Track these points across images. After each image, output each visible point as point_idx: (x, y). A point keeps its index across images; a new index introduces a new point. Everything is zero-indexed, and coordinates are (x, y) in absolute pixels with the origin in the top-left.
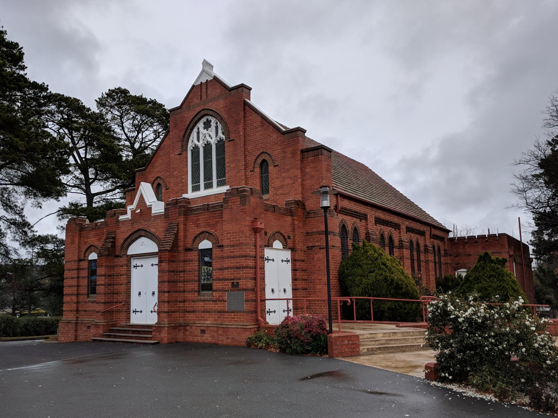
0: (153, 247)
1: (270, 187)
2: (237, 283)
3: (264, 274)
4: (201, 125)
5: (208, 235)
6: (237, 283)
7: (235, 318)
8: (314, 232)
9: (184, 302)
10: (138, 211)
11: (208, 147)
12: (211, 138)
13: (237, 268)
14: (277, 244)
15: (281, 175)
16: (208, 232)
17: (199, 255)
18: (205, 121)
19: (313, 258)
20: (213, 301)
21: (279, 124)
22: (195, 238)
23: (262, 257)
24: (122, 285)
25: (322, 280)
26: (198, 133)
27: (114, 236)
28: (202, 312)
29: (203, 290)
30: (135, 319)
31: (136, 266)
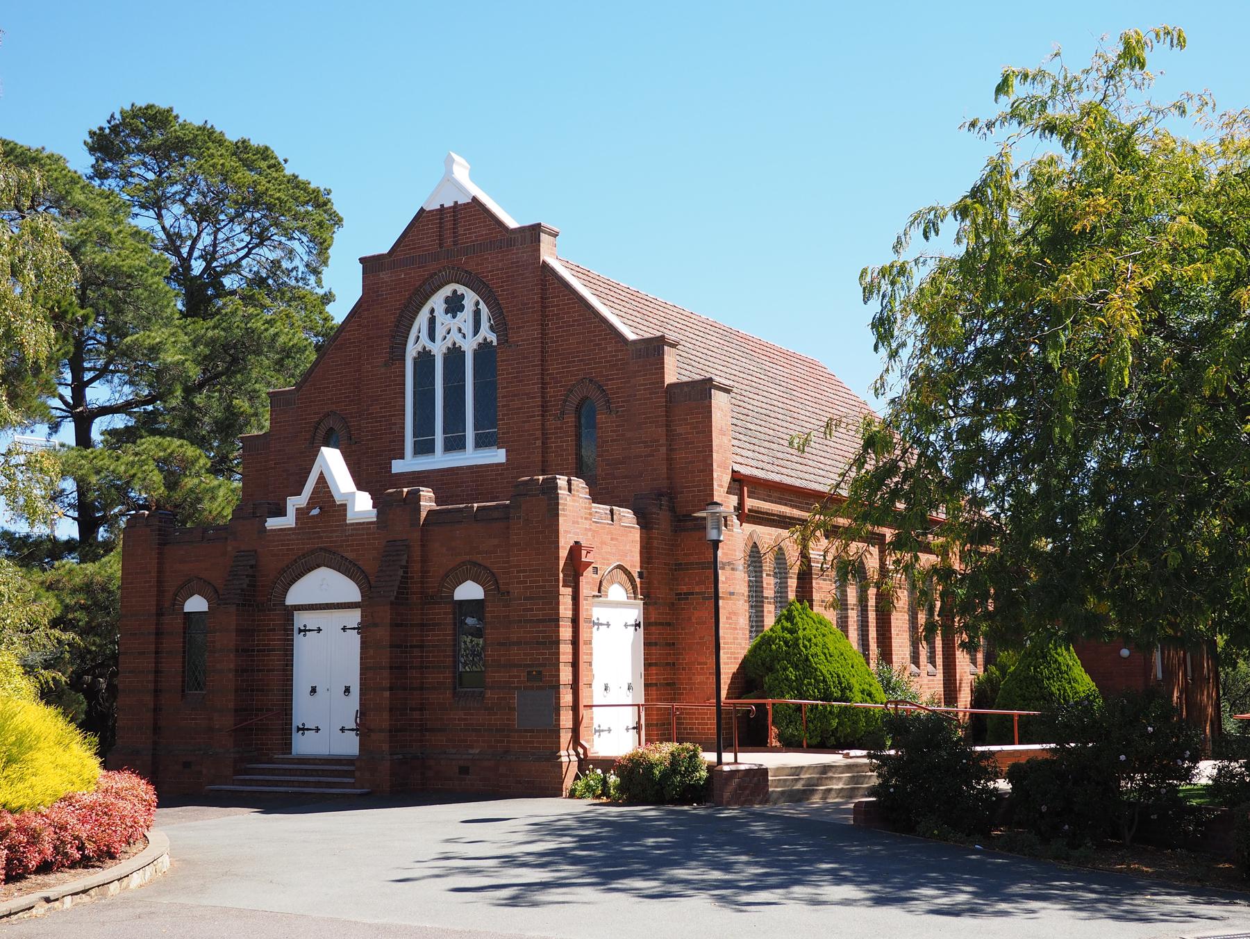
0: (349, 591)
2: (540, 673)
4: (437, 301)
7: (532, 742)
8: (692, 564)
9: (421, 710)
10: (315, 512)
12: (464, 336)
17: (454, 613)
19: (690, 618)
24: (273, 670)
26: (432, 321)
27: (253, 562)
30: (304, 745)
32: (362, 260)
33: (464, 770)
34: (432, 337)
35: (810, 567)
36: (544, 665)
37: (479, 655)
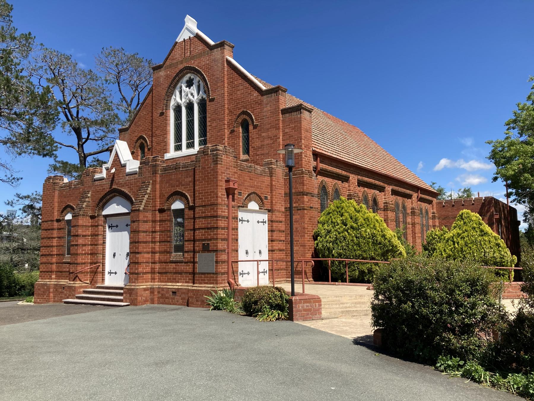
1: (250, 147)
3: (237, 235)
6: (208, 244)
11: (190, 107)
12: (193, 97)
13: (208, 228)
14: (253, 205)
15: (261, 135)
20: (185, 263)
23: (236, 218)
25: (299, 241)
36: (210, 240)
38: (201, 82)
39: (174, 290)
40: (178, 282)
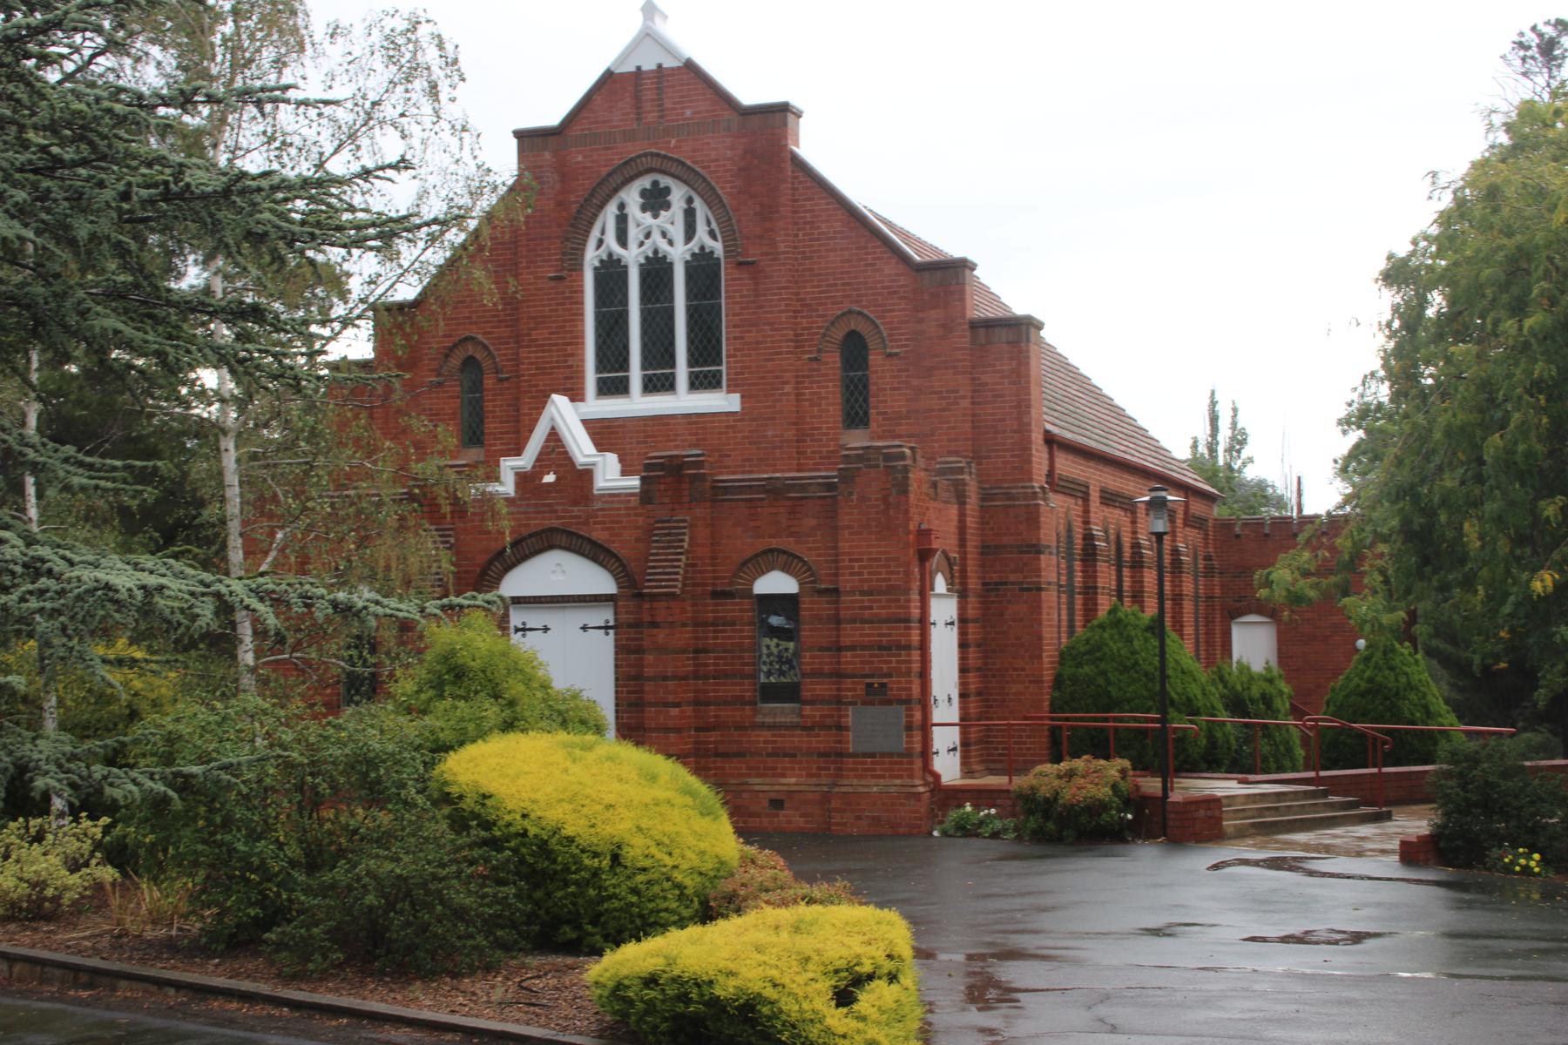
0: (599, 581)
4: (632, 196)
5: (788, 562)
6: (883, 685)
13: (881, 648)
16: (784, 552)
18: (648, 186)
19: (1002, 615)
20: (804, 728)
21: (876, 215)
22: (744, 564)
25: (1023, 669)
26: (622, 220)
28: (769, 755)
29: (765, 699)
31: (524, 630)
32: (520, 135)
33: (777, 804)
34: (622, 239)
35: (1141, 555)
36: (889, 675)
37: (789, 661)
38: (698, 204)
39: (773, 795)
40: (784, 776)
